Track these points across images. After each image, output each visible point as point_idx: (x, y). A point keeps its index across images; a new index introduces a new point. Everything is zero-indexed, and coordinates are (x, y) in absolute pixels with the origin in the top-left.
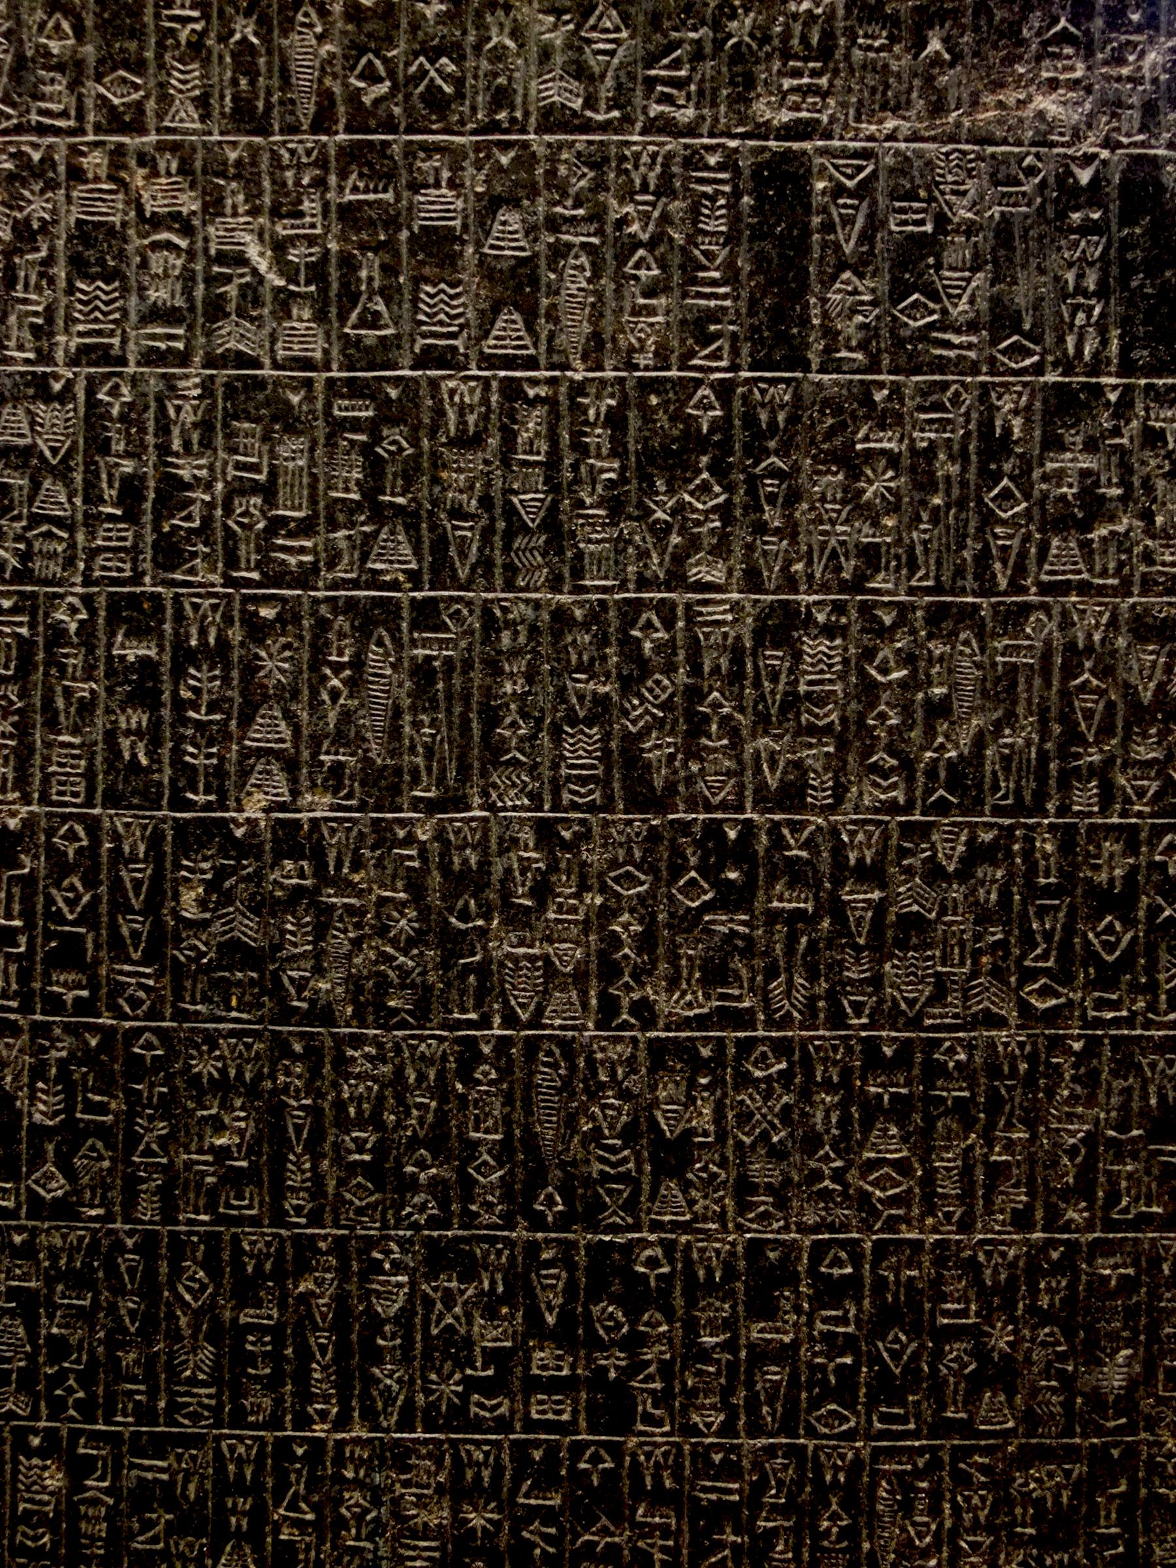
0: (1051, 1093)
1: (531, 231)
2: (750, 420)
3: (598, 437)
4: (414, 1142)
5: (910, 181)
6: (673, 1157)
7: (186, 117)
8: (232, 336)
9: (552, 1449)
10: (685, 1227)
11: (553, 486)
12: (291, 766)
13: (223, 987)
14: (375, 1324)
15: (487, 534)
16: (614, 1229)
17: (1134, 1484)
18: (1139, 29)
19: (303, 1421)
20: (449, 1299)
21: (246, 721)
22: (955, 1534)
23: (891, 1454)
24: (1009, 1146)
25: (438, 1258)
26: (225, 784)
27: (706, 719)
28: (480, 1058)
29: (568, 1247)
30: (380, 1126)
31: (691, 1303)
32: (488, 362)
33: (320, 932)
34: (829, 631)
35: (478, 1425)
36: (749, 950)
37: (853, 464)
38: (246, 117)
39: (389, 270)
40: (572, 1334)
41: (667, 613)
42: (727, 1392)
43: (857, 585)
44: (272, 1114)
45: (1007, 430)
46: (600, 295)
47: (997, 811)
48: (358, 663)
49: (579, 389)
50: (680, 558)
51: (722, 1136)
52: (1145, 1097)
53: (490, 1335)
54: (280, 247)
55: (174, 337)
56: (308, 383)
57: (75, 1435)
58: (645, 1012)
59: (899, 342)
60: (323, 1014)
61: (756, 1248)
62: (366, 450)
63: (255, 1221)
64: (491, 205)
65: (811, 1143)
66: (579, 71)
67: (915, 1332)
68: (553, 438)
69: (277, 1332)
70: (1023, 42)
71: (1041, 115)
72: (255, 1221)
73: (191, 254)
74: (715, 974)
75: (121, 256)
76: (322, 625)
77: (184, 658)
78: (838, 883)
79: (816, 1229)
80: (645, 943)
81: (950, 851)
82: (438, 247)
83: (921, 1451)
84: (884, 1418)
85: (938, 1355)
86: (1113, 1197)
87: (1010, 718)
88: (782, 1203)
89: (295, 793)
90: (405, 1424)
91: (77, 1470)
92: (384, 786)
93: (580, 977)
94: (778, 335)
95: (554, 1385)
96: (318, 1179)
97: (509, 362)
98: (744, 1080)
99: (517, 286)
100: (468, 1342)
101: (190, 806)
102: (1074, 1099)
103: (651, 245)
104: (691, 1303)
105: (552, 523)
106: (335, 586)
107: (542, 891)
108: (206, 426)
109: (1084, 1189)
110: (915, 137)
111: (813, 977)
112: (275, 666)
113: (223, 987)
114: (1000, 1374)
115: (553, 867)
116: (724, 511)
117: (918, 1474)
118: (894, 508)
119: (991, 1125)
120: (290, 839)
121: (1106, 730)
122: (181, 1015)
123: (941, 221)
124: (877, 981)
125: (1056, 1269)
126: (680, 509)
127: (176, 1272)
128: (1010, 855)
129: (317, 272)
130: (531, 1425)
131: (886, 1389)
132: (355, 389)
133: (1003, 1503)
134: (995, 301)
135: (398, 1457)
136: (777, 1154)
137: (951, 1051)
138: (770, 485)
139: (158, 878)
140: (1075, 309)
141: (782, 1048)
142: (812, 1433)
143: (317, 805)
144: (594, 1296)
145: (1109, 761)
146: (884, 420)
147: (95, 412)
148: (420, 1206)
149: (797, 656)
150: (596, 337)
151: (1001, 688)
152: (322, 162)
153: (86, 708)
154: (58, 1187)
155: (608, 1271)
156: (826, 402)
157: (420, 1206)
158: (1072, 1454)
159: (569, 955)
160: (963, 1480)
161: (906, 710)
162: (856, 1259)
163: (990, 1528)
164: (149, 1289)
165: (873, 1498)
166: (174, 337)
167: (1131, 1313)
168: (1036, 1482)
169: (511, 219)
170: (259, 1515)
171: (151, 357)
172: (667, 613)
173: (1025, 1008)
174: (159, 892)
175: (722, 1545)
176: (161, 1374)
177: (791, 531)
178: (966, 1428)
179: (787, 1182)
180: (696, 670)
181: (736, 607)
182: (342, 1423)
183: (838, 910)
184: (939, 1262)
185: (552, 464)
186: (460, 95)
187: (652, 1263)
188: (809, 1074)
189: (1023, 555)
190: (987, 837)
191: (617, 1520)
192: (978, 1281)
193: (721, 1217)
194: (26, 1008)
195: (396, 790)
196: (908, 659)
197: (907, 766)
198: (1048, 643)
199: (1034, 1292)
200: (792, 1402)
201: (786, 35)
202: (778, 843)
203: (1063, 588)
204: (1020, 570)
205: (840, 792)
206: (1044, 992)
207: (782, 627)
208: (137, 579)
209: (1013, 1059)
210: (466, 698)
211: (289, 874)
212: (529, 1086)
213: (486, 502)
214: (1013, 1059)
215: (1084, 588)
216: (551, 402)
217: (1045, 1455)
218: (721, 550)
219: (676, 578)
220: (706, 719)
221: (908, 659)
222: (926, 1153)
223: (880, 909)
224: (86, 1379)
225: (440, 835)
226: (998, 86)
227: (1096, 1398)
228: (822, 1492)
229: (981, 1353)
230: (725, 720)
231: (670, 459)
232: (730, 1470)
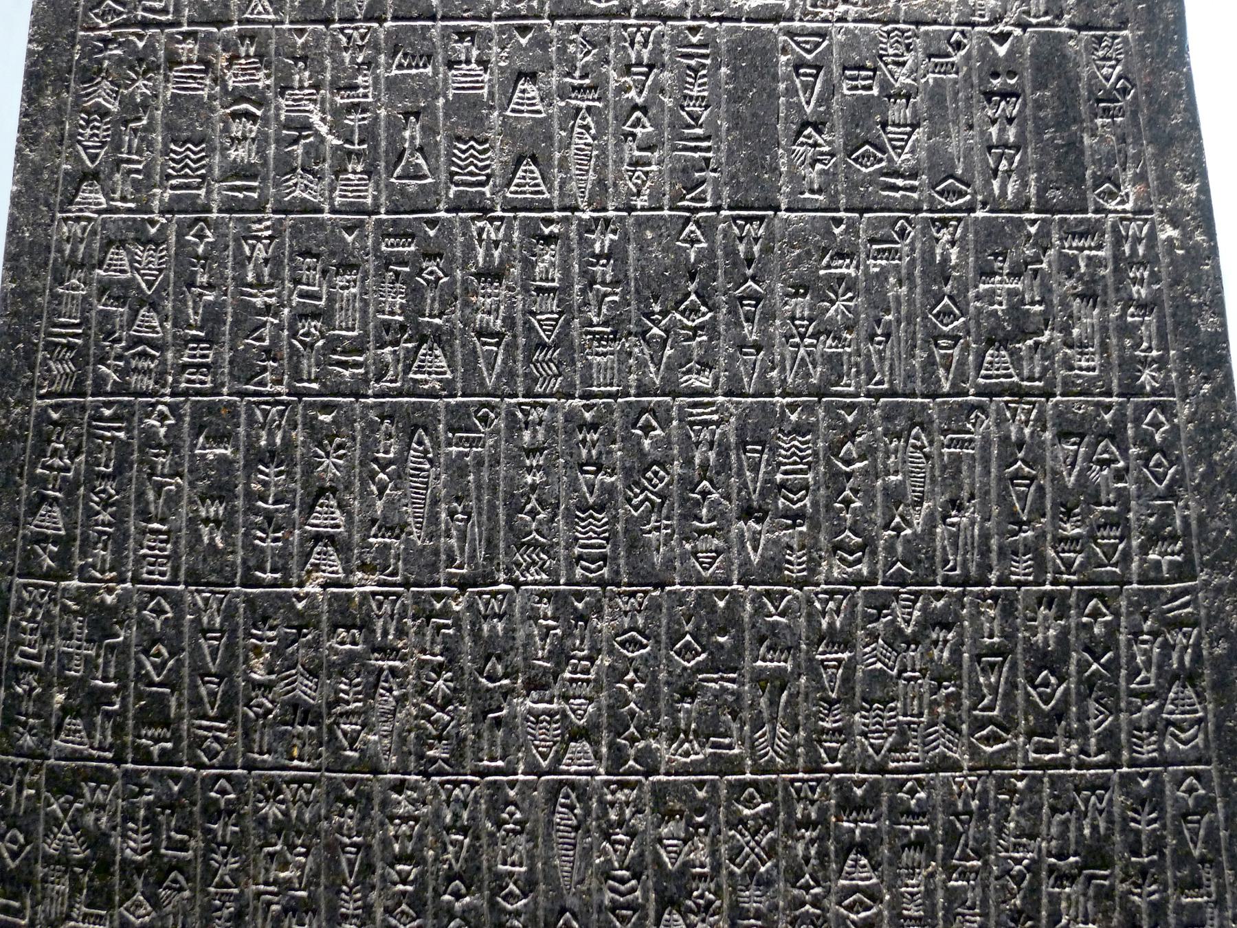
2: (731, 253)
45: (946, 259)
51: (717, 867)
74: (708, 730)
89: (348, 572)
101: (259, 583)
108: (274, 261)
122: (250, 766)
129: (368, 134)
137: (912, 792)
141: (766, 791)
161: (869, 496)
183: (814, 669)
194: (118, 760)
195: (434, 567)
208: (215, 392)
210: (494, 489)
211: (342, 643)
225: (471, 606)
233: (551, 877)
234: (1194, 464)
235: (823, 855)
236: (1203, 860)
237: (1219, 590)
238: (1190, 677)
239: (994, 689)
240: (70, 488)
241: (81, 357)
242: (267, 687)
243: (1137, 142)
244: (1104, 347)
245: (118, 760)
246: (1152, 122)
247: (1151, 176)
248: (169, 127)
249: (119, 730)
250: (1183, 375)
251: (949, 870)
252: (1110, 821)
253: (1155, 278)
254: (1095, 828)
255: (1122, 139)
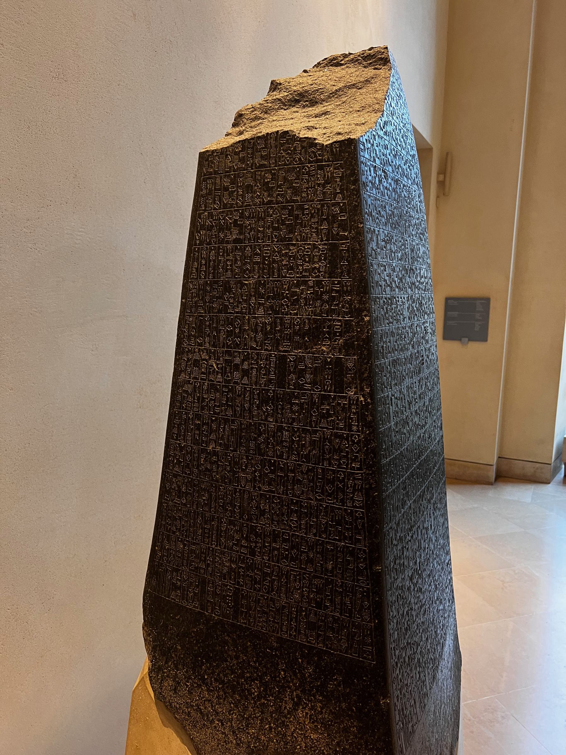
0: (320, 514)
1: (249, 365)
2: (277, 396)
3: (256, 397)
4: (228, 503)
5: (301, 359)
6: (262, 513)
7: (207, 345)
8: (212, 377)
9: (244, 557)
10: (264, 525)
11: (250, 404)
12: (215, 442)
13: (205, 474)
14: (222, 531)
15: (241, 410)
16: (254, 523)
17: (333, 586)
18: (338, 336)
19: (212, 545)
20: (232, 529)
21: (210, 434)
22: (303, 587)
23: (293, 571)
24: (313, 521)
25: (231, 523)
26: (208, 445)
27: (270, 442)
28: (237, 492)
29: (248, 524)
30: (224, 500)
31: (264, 538)
32: (242, 384)
33: (218, 468)
34: (287, 431)
35: (234, 551)
36: (274, 481)
37: (292, 404)
38: (214, 346)
39: (231, 369)
40: (247, 539)
41: (265, 424)
42: (269, 554)
43: (291, 424)
44: (210, 496)
45: (315, 400)
46: (257, 375)
47: (312, 464)
48: (224, 428)
49: (254, 389)
50: (266, 417)
51: (270, 510)
52: (336, 518)
53: (237, 537)
54: (217, 365)
55: (204, 376)
56: (220, 385)
57: (184, 540)
58: (260, 489)
59: (299, 385)
60: (217, 481)
61: (274, 530)
62: (227, 395)
63: (207, 511)
64: (243, 361)
65: (283, 515)
66: (256, 341)
67: (297, 550)
68: (250, 397)
69: (209, 529)
70: (320, 338)
71: (322, 350)
72: (207, 511)
73: (207, 365)
74: (270, 484)
75: (199, 364)
76: (220, 421)
77: (204, 424)
78: (288, 472)
79: (283, 529)
80: (260, 477)
81: (304, 469)
82: (237, 367)
83: (298, 571)
84: (292, 564)
85: (301, 555)
86: (330, 534)
87: (314, 449)
88: (278, 524)
89: (216, 446)
90: (225, 548)
91: (185, 545)
92: (227, 447)
93: (251, 481)
94: (281, 383)
95: (245, 547)
96: (216, 506)
97: (245, 384)
98: (273, 502)
99: (246, 373)
100: (234, 537)
101: (203, 446)
102: (324, 515)
103: (264, 368)
104: (264, 538)
105: (249, 409)
106: (222, 415)
107: (246, 466)
108: (207, 390)
109: (325, 532)
110: (303, 353)
111: (284, 487)
112: (214, 426)
113: (205, 474)
114: (310, 561)
115: (248, 463)
116: (273, 410)
117: (297, 575)
118: (297, 412)
119: (310, 517)
120: (215, 453)
121: (329, 453)
122: (200, 478)
123: (306, 366)
124: (293, 489)
125: (320, 545)
126: (267, 409)
127: (198, 517)
128: (314, 472)
129: (222, 369)
130: (241, 553)
131: (293, 559)
132: (226, 386)
133: (310, 584)
134: (314, 380)
135: (223, 553)
136: (278, 515)
137: (304, 503)
138: (280, 406)
139: (199, 456)
140: (327, 382)
141: (279, 498)
142: (281, 564)
143: (218, 449)
144: (251, 534)
145: (330, 457)
146: (297, 397)
147: (195, 386)
148: (228, 514)
149: (283, 434)
150: (256, 381)
151: (313, 443)
152: (223, 353)
153: (192, 429)
154: (184, 502)
155: (253, 530)
156: (288, 394)
157: (228, 514)
158: (322, 578)
159: (249, 477)
160: (304, 578)
161: (298, 445)
162: (289, 535)
163: (308, 588)
164: (194, 519)
165: (290, 578)
166: (204, 376)
167: (333, 555)
168: (315, 581)
169: (246, 363)
170: (205, 558)
171: (202, 379)
172: (265, 424)
173: (316, 498)
174: (199, 458)
175: (267, 580)
176: (195, 532)
177: (282, 414)
178: (305, 569)
179: (279, 520)
180: (268, 435)
181: (274, 425)
182: (216, 546)
183: (288, 476)
184: (302, 539)
185: (250, 400)
186: (240, 344)
187: (259, 529)
188: (283, 503)
189: (317, 421)
190: (310, 468)
191: (252, 571)
192: (307, 544)
193: (269, 524)
194: (182, 473)
195: (228, 447)
196: (299, 436)
197: (298, 454)
198: (321, 436)
199: (317, 548)
200: (278, 559)
201: (284, 337)
202: (279, 464)
203: (324, 428)
204: (316, 424)
205: (288, 457)
206: (319, 496)
207: (280, 429)
208: (198, 412)
209: (314, 507)
210: (238, 435)
211: (214, 458)
212: (243, 497)
213: (241, 405)
214: (314, 507)
215: (326, 428)
216: (250, 391)
217: (318, 577)
218: (272, 416)
219: (266, 420)
220: (270, 442)
221: (299, 436)
222: (300, 520)
223: (294, 477)
224: (186, 531)
225: (233, 455)
226: (316, 345)
227: (327, 570)
228: (282, 575)
229: (308, 556)
230: (272, 443)
231: (265, 401)
232: (269, 567)
233: (243, 506)
234: (364, 447)
235: (288, 512)
236: (361, 529)
237: (368, 474)
238: (361, 491)
239: (320, 486)
240: (178, 425)
241: (181, 403)
242: (203, 464)
243: (356, 380)
244: (345, 422)
245: (182, 473)
246: (359, 376)
247: (359, 387)
248: (194, 364)
249: (183, 468)
250: (362, 429)
251: (310, 520)
252: (342, 517)
253: (357, 408)
254: (338, 518)
255: (353, 379)
